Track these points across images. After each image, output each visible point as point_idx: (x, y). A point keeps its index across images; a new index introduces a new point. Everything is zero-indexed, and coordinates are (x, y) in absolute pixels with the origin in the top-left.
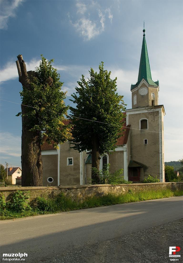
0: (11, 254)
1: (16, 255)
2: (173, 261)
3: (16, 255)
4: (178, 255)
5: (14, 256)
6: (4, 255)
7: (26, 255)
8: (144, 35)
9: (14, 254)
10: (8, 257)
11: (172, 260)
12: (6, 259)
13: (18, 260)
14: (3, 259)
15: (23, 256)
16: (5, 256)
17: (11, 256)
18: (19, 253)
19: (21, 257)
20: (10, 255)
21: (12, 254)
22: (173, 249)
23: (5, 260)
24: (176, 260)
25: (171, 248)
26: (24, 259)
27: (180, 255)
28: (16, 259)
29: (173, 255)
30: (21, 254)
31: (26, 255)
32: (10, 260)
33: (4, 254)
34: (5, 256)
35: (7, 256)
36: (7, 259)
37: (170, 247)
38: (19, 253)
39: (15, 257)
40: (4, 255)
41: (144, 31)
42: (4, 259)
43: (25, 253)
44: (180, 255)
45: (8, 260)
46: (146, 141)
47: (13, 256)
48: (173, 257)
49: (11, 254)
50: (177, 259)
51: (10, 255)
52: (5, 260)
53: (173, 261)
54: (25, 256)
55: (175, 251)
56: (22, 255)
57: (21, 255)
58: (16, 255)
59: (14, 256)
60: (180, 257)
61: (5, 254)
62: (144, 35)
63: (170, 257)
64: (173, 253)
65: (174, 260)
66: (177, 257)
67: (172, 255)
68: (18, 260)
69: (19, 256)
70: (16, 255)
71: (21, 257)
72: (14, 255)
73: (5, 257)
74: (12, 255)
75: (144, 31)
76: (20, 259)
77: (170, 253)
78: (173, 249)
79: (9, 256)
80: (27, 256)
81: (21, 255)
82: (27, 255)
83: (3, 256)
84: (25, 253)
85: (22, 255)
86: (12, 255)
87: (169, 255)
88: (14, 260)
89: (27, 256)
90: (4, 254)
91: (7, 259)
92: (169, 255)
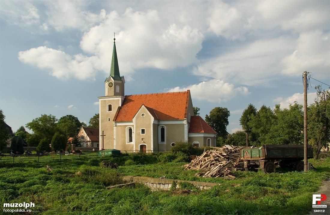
0: (14, 204)
1: (21, 205)
2: (317, 212)
3: (21, 205)
4: (324, 206)
5: (18, 206)
6: (6, 205)
7: (32, 205)
8: (115, 42)
9: (17, 204)
10: (10, 208)
11: (316, 212)
12: (8, 210)
13: (22, 211)
14: (4, 210)
15: (29, 206)
16: (7, 206)
17: (13, 206)
18: (24, 203)
19: (26, 208)
20: (12, 205)
21: (16, 204)
22: (317, 198)
23: (6, 211)
24: (321, 211)
25: (314, 196)
27: (326, 205)
28: (21, 211)
29: (317, 205)
30: (26, 204)
31: (32, 205)
32: (13, 211)
33: (5, 204)
34: (7, 206)
35: (9, 206)
36: (8, 210)
37: (313, 195)
38: (24, 203)
39: (19, 208)
40: (6, 205)
41: (115, 39)
42: (5, 210)
43: (31, 203)
44: (326, 205)
45: (11, 211)
46: (109, 121)
47: (16, 206)
48: (318, 207)
49: (14, 204)
50: (322, 210)
51: (12, 205)
52: (6, 211)
53: (317, 212)
54: (31, 206)
55: (320, 200)
56: (28, 205)
57: (26, 205)
58: (21, 205)
59: (18, 206)
61: (7, 204)
62: (115, 42)
63: (314, 207)
64: (318, 203)
65: (318, 211)
66: (323, 207)
67: (316, 205)
68: (22, 211)
69: (24, 206)
70: (21, 205)
71: (26, 208)
72: (18, 205)
73: (6, 208)
74: (15, 205)
75: (115, 39)
76: (26, 210)
77: (314, 202)
78: (317, 198)
79: (11, 206)
80: (34, 206)
81: (26, 205)
82: (34, 204)
83: (4, 206)
84: (31, 203)
85: (28, 205)
86: (15, 205)
87: (313, 205)
88: (17, 211)
89: (34, 206)
90: (5, 204)
91: (8, 210)
92: (313, 205)
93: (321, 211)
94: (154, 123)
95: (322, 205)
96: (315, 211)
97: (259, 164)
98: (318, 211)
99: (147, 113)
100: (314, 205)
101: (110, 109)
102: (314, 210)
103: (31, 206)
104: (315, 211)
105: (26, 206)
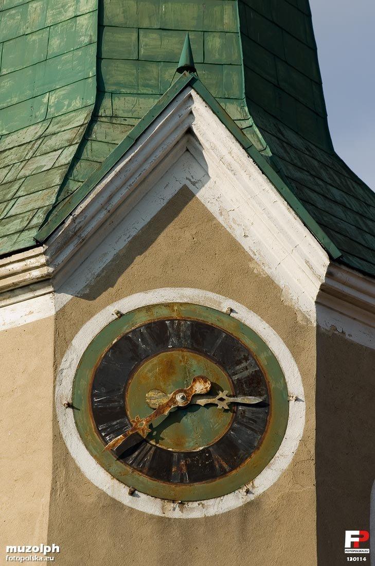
0: (23, 547)
4: (364, 550)
7: (56, 549)
11: (351, 560)
15: (49, 551)
17: (23, 550)
22: (353, 536)
24: (360, 559)
26: (52, 558)
29: (353, 550)
31: (56, 549)
34: (11, 551)
44: (369, 550)
48: (354, 552)
49: (23, 547)
50: (358, 558)
54: (53, 551)
55: (357, 540)
56: (47, 549)
60: (369, 552)
61: (12, 548)
63: (347, 552)
64: (353, 545)
65: (355, 559)
67: (351, 550)
77: (348, 544)
78: (353, 536)
80: (58, 551)
82: (58, 548)
84: (53, 545)
85: (47, 549)
87: (346, 550)
89: (58, 551)
90: (8, 548)
92: (346, 550)
93: (360, 559)
94: (326, 327)
95: (362, 550)
96: (350, 559)
97: (3, 73)
98: (355, 559)
99: (239, 41)
100: (347, 550)
101: (263, 264)
102: (348, 558)
103: (53, 551)
104: (350, 559)
105: (45, 551)
